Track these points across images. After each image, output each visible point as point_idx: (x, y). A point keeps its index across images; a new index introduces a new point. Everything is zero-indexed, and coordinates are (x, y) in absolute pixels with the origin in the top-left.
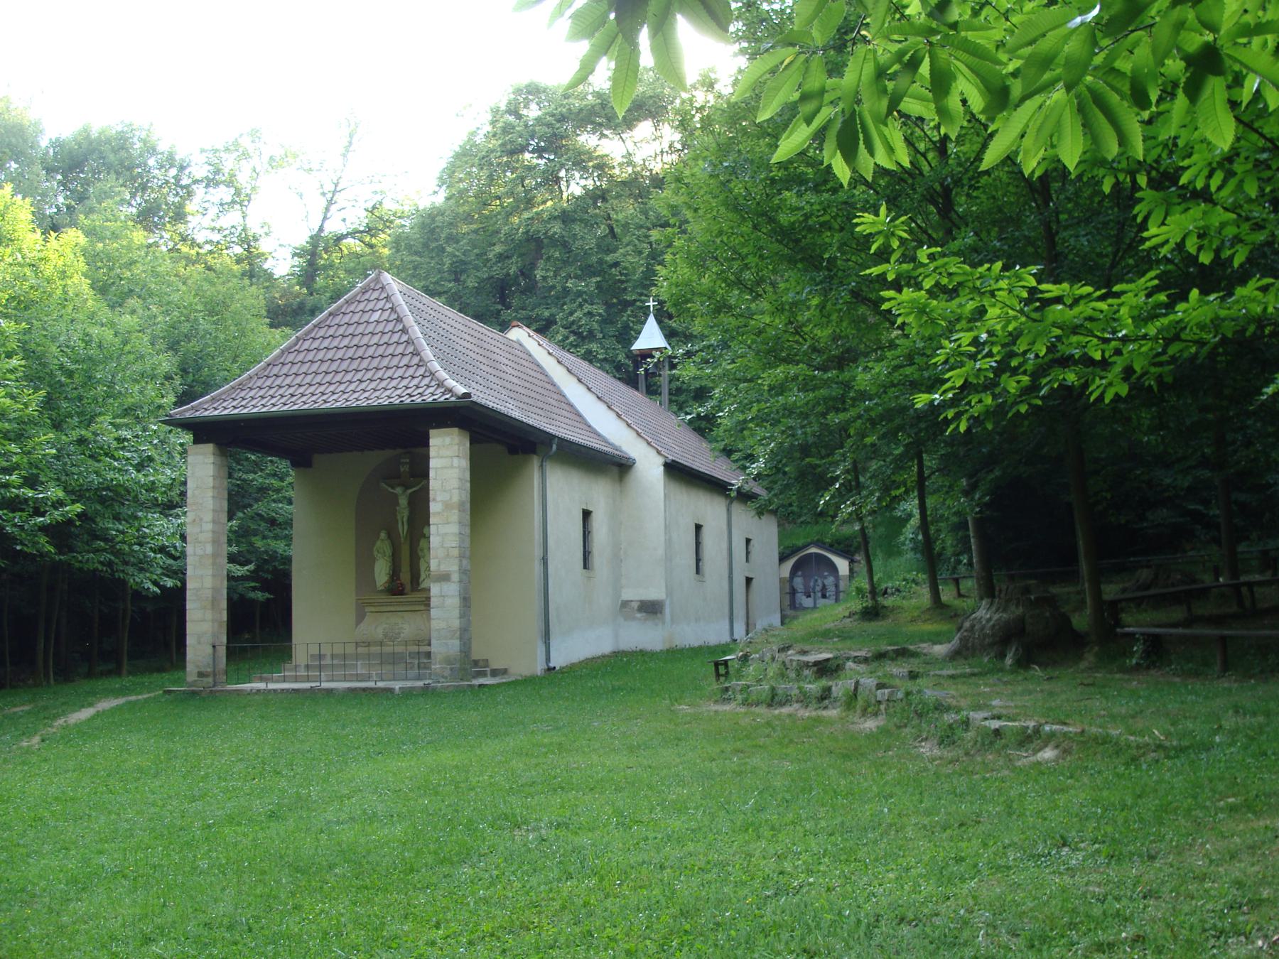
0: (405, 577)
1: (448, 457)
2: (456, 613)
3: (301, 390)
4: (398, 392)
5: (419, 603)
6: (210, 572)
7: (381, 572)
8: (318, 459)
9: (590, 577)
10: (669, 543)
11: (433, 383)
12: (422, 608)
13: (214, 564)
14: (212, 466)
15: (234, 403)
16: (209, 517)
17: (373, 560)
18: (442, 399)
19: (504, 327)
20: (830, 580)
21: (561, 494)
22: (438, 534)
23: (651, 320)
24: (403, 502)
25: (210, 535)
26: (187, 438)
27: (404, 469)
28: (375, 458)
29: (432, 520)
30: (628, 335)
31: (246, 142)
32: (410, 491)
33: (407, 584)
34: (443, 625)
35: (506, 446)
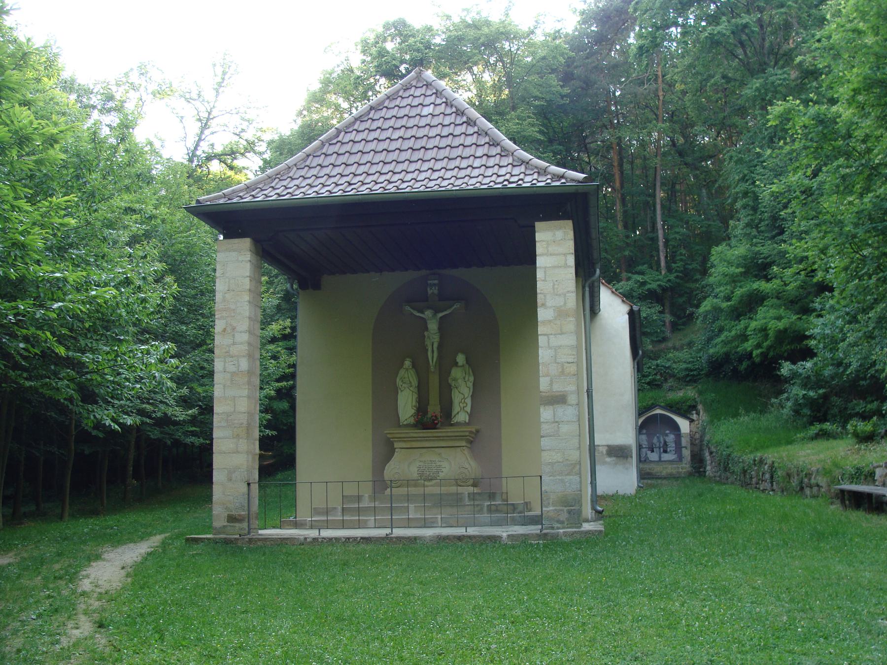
0: (434, 409)
6: (245, 392)
7: (406, 405)
8: (327, 280)
14: (248, 265)
16: (244, 325)
17: (395, 391)
20: (671, 438)
22: (550, 347)
24: (433, 326)
25: (245, 347)
27: (433, 291)
29: (541, 329)
31: (134, 78)
32: (441, 315)
34: (558, 457)
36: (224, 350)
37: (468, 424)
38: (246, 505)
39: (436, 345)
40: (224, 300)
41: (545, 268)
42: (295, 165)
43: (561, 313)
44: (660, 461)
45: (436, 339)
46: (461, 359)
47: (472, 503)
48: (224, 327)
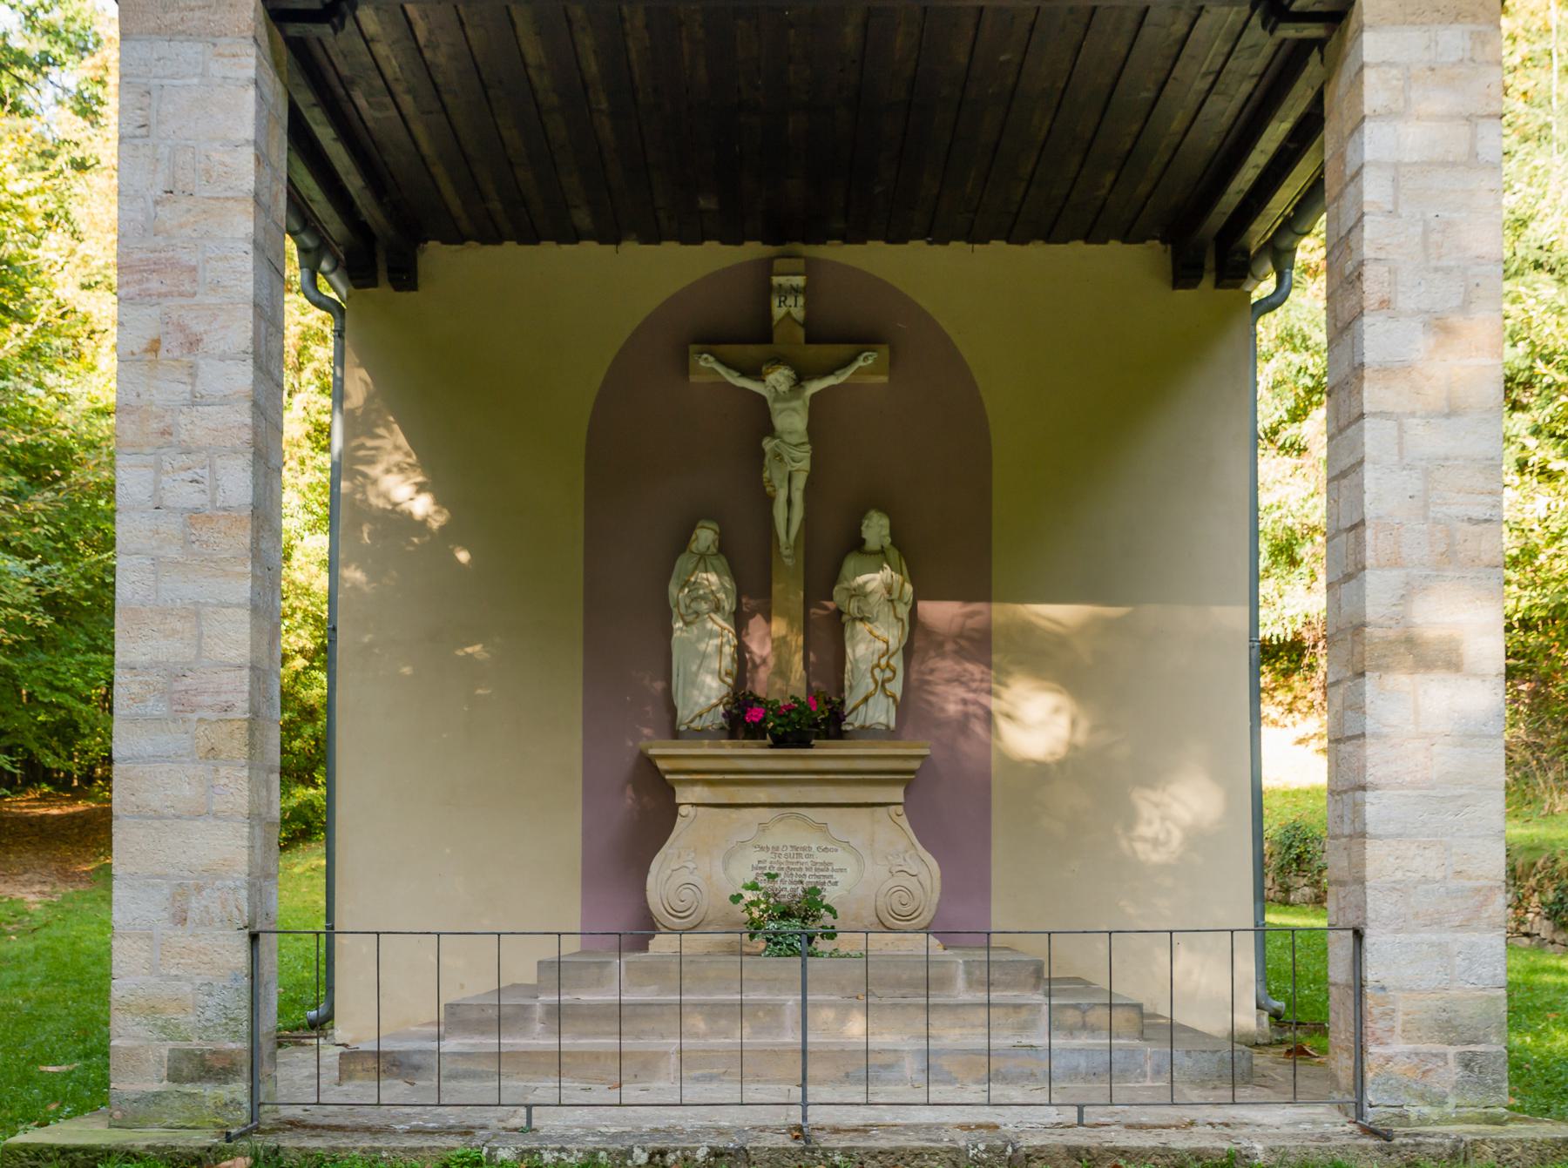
24: (792, 420)
36: (155, 425)
37: (890, 734)
38: (244, 1014)
39: (800, 482)
41: (1396, 166)
45: (801, 462)
46: (876, 529)
47: (981, 996)
48: (151, 333)
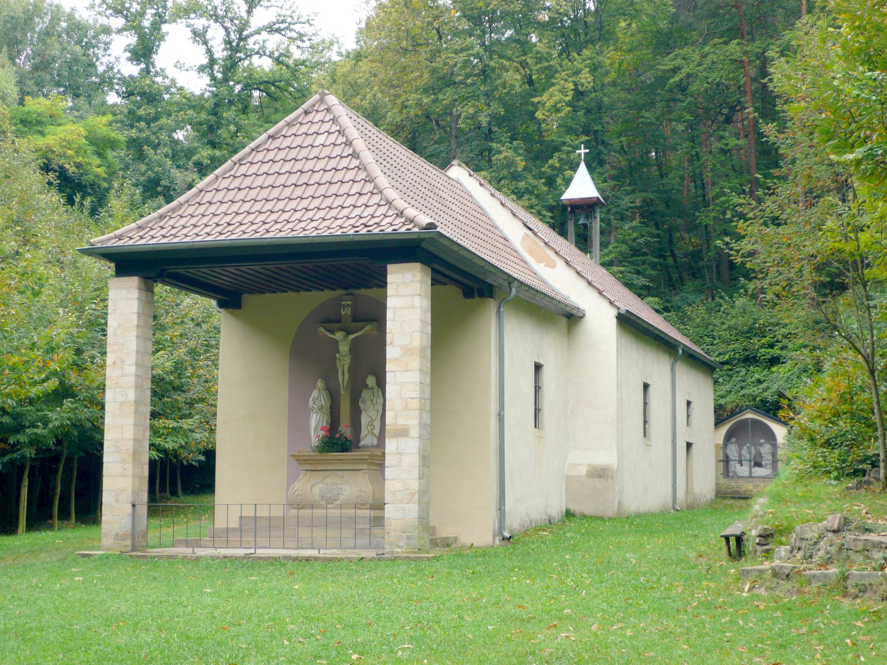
0: (345, 429)
1: (407, 295)
2: (415, 473)
3: (239, 218)
4: (351, 222)
5: (377, 464)
9: (540, 437)
10: (620, 401)
11: (390, 213)
12: (379, 468)
13: (136, 412)
14: (136, 303)
15: (163, 232)
16: (132, 359)
18: (403, 230)
19: (444, 165)
21: (512, 345)
23: (583, 169)
24: (344, 348)
25: (132, 379)
26: (109, 268)
27: (346, 312)
28: (315, 299)
30: (556, 180)
33: (345, 440)
35: (466, 283)
39: (346, 367)
40: (115, 335)
42: (187, 202)
43: (407, 351)
44: (751, 477)
